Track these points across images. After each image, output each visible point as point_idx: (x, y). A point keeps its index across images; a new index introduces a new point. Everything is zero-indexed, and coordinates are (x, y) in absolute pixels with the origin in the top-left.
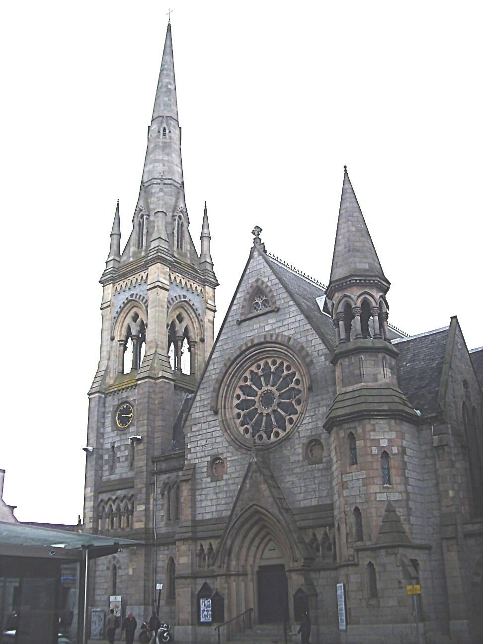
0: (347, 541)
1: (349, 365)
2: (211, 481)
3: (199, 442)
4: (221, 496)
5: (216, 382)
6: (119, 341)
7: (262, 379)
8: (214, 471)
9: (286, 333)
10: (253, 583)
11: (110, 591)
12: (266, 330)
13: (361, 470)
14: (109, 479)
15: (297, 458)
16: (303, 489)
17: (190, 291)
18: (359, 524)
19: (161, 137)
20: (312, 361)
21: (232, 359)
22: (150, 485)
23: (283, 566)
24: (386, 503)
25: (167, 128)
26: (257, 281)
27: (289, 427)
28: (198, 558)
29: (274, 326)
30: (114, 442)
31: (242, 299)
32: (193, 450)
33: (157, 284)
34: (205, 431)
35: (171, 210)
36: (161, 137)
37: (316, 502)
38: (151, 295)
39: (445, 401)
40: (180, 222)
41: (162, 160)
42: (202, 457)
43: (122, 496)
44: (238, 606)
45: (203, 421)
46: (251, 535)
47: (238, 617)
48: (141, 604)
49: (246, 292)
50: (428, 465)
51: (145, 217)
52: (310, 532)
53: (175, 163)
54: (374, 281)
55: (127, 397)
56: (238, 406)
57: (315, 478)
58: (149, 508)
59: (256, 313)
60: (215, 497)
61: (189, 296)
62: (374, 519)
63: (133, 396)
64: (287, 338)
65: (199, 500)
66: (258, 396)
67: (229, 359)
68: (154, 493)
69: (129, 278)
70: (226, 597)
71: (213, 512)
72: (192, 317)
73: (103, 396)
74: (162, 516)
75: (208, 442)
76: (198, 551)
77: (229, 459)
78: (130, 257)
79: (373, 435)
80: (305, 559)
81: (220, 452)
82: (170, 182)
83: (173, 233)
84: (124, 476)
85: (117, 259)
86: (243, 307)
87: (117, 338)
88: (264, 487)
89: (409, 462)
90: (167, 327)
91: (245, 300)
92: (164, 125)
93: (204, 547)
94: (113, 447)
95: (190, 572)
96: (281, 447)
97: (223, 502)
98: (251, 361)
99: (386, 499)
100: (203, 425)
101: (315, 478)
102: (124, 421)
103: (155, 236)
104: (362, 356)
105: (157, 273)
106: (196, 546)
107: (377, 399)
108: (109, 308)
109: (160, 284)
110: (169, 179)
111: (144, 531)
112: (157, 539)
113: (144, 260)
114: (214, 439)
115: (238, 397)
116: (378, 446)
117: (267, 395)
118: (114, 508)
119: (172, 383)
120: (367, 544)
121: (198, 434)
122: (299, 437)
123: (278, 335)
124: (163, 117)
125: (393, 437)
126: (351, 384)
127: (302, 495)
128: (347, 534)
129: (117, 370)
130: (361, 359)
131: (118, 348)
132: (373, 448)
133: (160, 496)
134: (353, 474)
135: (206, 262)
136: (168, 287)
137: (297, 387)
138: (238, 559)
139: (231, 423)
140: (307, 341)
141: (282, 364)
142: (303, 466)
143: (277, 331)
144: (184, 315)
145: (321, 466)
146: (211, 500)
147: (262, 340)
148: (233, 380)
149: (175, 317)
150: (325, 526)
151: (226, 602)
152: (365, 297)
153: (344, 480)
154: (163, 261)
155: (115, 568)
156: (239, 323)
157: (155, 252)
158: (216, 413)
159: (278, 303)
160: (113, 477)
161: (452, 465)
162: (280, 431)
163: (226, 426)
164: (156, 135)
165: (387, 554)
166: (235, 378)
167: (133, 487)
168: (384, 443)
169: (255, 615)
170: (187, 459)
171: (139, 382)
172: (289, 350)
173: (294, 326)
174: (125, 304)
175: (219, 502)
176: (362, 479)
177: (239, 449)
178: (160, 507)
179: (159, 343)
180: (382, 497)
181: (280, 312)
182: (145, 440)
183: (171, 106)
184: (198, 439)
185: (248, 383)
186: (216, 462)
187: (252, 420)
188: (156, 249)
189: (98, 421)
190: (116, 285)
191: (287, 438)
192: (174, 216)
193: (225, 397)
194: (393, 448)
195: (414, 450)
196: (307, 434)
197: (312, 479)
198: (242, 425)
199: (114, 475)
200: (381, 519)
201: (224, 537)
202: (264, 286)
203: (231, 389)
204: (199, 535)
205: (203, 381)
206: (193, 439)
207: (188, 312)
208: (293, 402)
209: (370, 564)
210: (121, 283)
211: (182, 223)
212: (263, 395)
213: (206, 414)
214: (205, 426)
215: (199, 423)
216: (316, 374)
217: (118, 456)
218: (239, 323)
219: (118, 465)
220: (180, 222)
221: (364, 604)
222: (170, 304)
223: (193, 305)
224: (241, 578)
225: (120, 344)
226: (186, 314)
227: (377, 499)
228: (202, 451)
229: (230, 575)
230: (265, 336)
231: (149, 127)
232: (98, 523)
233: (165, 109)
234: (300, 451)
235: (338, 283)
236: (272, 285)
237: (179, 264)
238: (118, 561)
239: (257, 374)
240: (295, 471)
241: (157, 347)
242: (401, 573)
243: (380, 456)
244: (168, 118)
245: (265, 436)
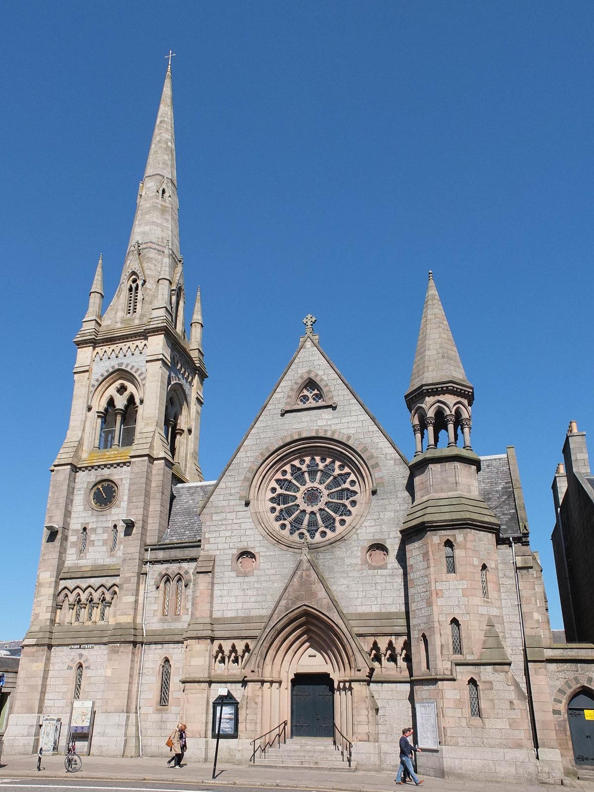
0: (441, 653)
4: (249, 592)
5: (249, 471)
6: (97, 412)
9: (345, 431)
11: (71, 694)
15: (354, 561)
16: (361, 594)
24: (487, 618)
26: (309, 372)
29: (329, 423)
30: (88, 524)
31: (288, 389)
32: (212, 540)
34: (230, 522)
41: (161, 224)
46: (291, 638)
48: (123, 712)
49: (293, 381)
60: (242, 593)
69: (117, 345)
74: (155, 610)
77: (262, 554)
84: (101, 562)
86: (289, 397)
91: (291, 390)
95: (206, 675)
97: (252, 599)
100: (228, 514)
108: (87, 374)
112: (146, 636)
113: (144, 328)
120: (468, 658)
121: (220, 523)
129: (92, 444)
131: (95, 420)
137: (351, 488)
143: (333, 428)
145: (384, 572)
150: (391, 635)
155: (80, 666)
160: (82, 562)
170: (204, 549)
173: (356, 425)
175: (247, 598)
178: (153, 600)
180: (483, 610)
190: (98, 349)
196: (369, 538)
200: (483, 633)
202: (291, 393)
204: (217, 634)
205: (230, 468)
209: (472, 682)
213: (232, 503)
214: (233, 515)
217: (92, 539)
219: (91, 549)
221: (464, 724)
234: (359, 554)
235: (432, 387)
238: (87, 660)
239: (300, 469)
242: (513, 693)
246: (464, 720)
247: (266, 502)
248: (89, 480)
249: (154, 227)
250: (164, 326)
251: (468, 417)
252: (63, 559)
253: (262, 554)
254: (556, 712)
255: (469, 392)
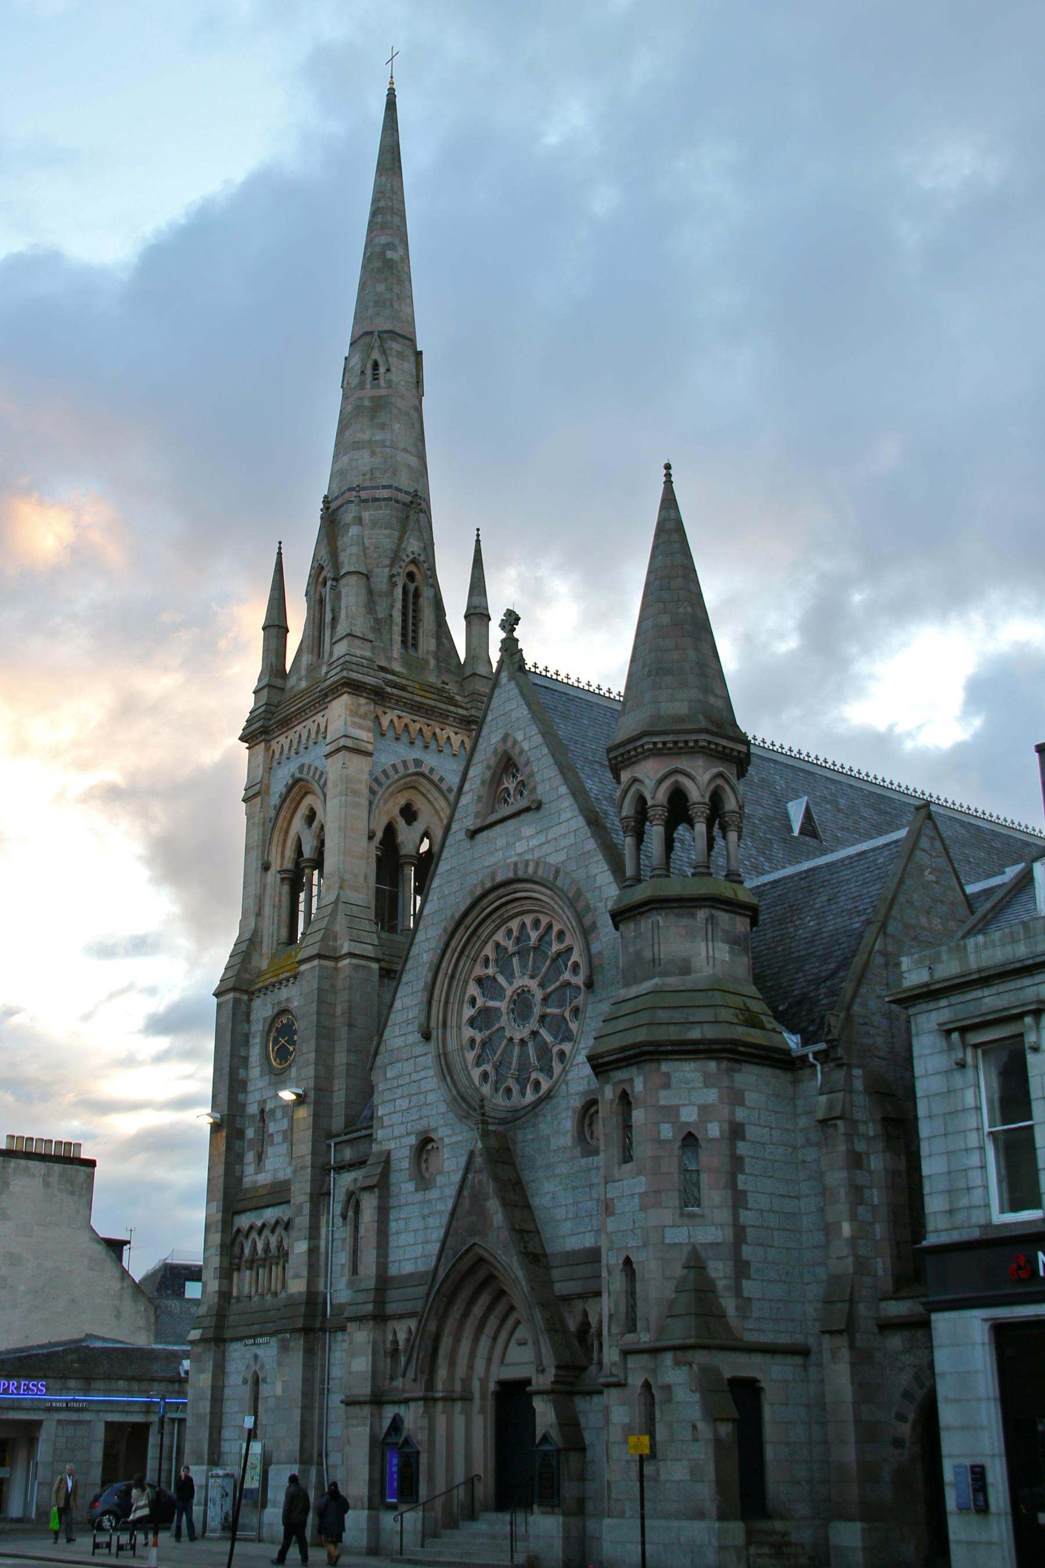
1: (636, 937)
2: (417, 1190)
3: (398, 1102)
7: (515, 960)
8: (424, 1166)
9: (552, 860)
10: (485, 1421)
12: (518, 852)
13: (639, 1174)
14: (256, 1182)
17: (433, 746)
18: (632, 1293)
19: (368, 386)
20: (594, 923)
21: (457, 916)
22: (320, 1195)
23: (528, 1382)
25: (380, 362)
26: (505, 738)
27: (557, 1068)
28: (389, 1360)
32: (386, 1121)
33: (343, 742)
34: (407, 1079)
35: (387, 562)
36: (368, 386)
37: (413, 1266)
38: (334, 769)
39: (849, 1017)
40: (412, 587)
41: (370, 441)
42: (401, 1137)
43: (273, 1221)
44: (450, 1469)
45: (405, 1057)
46: (478, 1310)
47: (449, 1491)
48: (295, 1463)
50: (809, 1162)
51: (329, 583)
52: (578, 1304)
53: (401, 446)
54: (696, 741)
55: (288, 1000)
56: (472, 1022)
57: (591, 1186)
58: (318, 1247)
59: (505, 810)
61: (430, 760)
62: (657, 1284)
63: (296, 997)
64: (554, 869)
65: (394, 1230)
66: (507, 999)
67: (452, 917)
68: (328, 1213)
70: (423, 1449)
71: (417, 1258)
72: (438, 808)
73: (245, 997)
75: (412, 1104)
76: (388, 1345)
78: (301, 679)
79: (665, 1098)
80: (558, 1367)
81: (433, 1125)
82: (385, 493)
83: (391, 616)
85: (278, 682)
87: (275, 866)
88: (493, 1205)
89: (752, 1157)
90: (371, 837)
91: (483, 783)
92: (376, 355)
93: (399, 1336)
94: (262, 1111)
96: (536, 1115)
98: (494, 921)
99: (686, 1241)
100: (405, 1064)
101: (591, 1186)
102: (283, 1054)
103: (342, 629)
104: (659, 918)
105: (340, 715)
106: (384, 1331)
107: (678, 1016)
108: (259, 799)
109: (349, 743)
110: (384, 487)
111: (304, 1298)
112: (331, 1315)
114: (422, 1097)
115: (473, 1001)
116: (675, 1122)
117: (522, 996)
118: (260, 1246)
119: (375, 966)
121: (396, 1084)
122: (568, 1094)
123: (537, 864)
124: (371, 333)
125: (710, 1101)
126: (636, 980)
127: (569, 1224)
128: (611, 1316)
129: (275, 938)
130: (655, 925)
132: (662, 1126)
133: (339, 1221)
134: (625, 1182)
135: (475, 674)
136: (370, 748)
138: (452, 1363)
139: (456, 1060)
140: (588, 877)
141: (550, 927)
142: (573, 1158)
143: (537, 855)
144: (420, 804)
146: (415, 1231)
147: (511, 875)
148: (461, 964)
149: (396, 811)
151: (423, 1459)
152: (677, 782)
153: (608, 1196)
154: (355, 687)
156: (473, 834)
157: (339, 668)
158: (427, 1036)
159: (540, 790)
161: (856, 1161)
162: (541, 1077)
163: (446, 1068)
164: (357, 380)
165: (678, 1363)
166: (464, 958)
167: (289, 1202)
168: (689, 1115)
169: (485, 1489)
171: (303, 968)
172: (556, 898)
174: (290, 788)
176: (640, 1194)
177: (464, 1120)
179: (347, 877)
181: (543, 811)
182: (312, 1094)
183: (391, 305)
184: (397, 1096)
185: (490, 971)
186: (425, 1145)
187: (495, 1054)
188: (341, 661)
189: (232, 1055)
191: (548, 1096)
192: (393, 576)
193: (447, 1003)
194: (710, 1125)
195: (771, 1128)
197: (587, 1189)
198: (478, 1064)
199: (263, 1174)
200: (672, 1285)
201: (422, 1316)
203: (458, 985)
206: (388, 1096)
207: (428, 795)
208: (567, 1014)
210: (282, 739)
211: (416, 590)
212: (515, 997)
214: (408, 1067)
215: (398, 1061)
216: (600, 953)
218: (473, 834)
220: (412, 587)
222: (380, 784)
223: (442, 779)
224: (458, 1406)
225: (283, 879)
226: (425, 802)
227: (666, 1241)
228: (403, 1123)
229: (435, 1400)
230: (516, 864)
231: (346, 359)
232: (232, 1280)
233: (377, 315)
235: (621, 750)
236: (530, 749)
237: (403, 688)
240: (558, 1171)
241: (341, 888)
243: (678, 1144)
244: (385, 335)
245: (516, 1089)
246: (633, 1464)
247: (463, 1028)
248: (265, 1015)
249: (356, 454)
250: (342, 678)
251: (737, 810)
252: (238, 1174)
253: (446, 1141)
254: (898, 1443)
255: (739, 752)
